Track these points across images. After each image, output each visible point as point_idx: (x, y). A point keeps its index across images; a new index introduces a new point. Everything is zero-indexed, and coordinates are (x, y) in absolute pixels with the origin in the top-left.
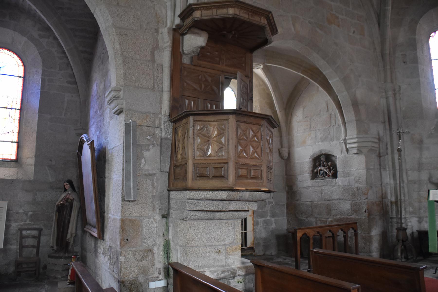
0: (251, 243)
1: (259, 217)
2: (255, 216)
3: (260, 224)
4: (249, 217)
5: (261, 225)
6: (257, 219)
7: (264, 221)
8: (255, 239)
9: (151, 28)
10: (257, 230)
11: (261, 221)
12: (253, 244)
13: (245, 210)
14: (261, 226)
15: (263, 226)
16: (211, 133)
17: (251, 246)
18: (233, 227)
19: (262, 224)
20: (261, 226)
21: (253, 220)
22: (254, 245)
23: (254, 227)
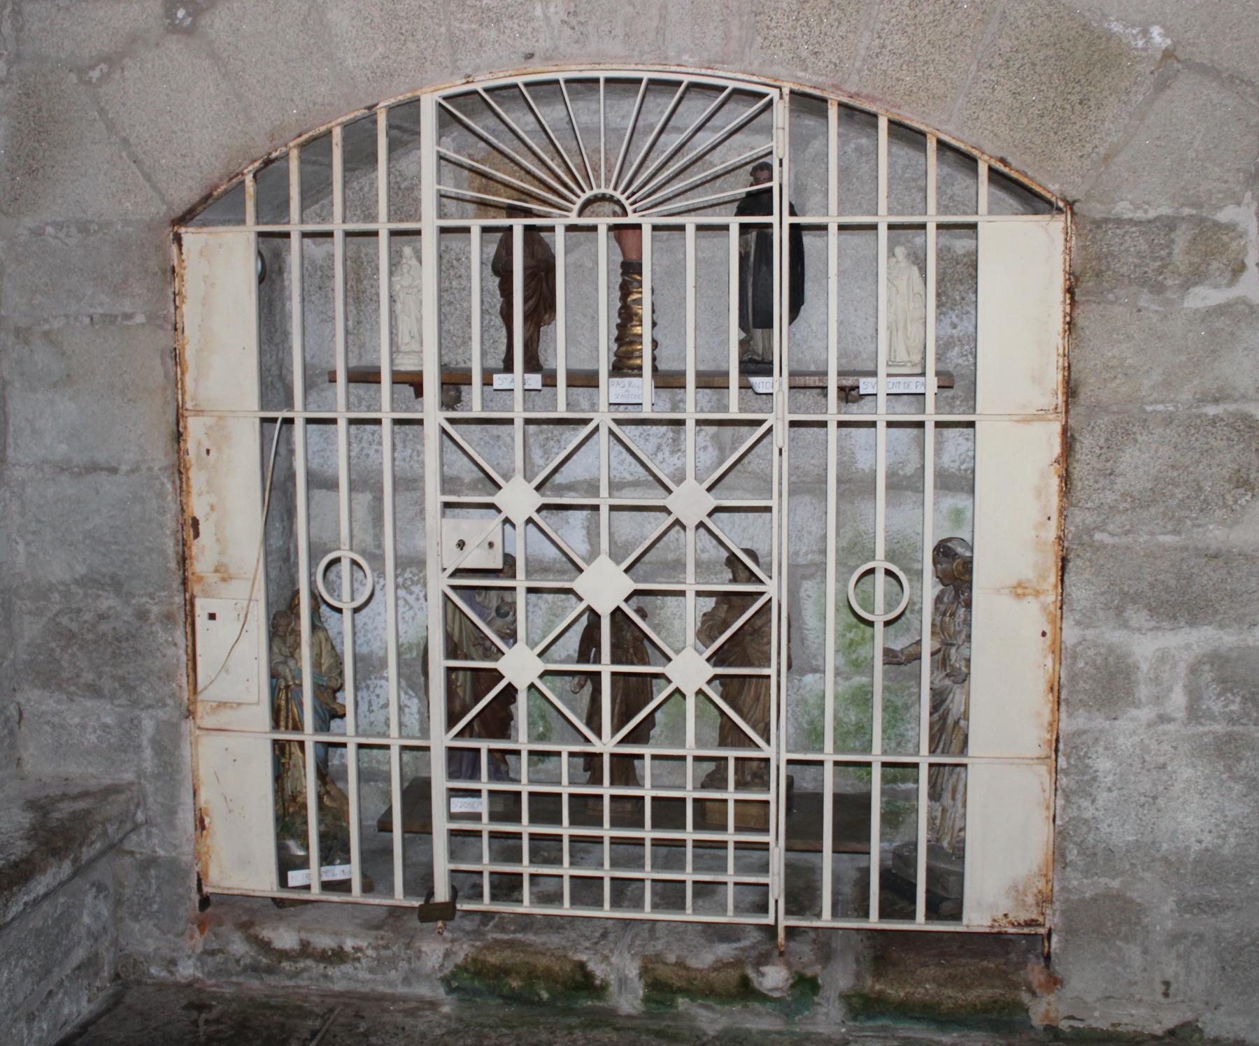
0: (1017, 892)
1: (1137, 617)
2: (1080, 592)
3: (1143, 691)
4: (1007, 601)
5: (1158, 700)
6: (1114, 636)
7: (1217, 659)
8: (1073, 854)
9: (168, 675)
10: (1103, 764)
11: (1163, 657)
12: (1045, 900)
13: (415, 753)
14: (1163, 719)
15: (1194, 713)
16: (188, 848)
17: (1023, 916)
18: (1063, 647)
19: (1178, 700)
20: (1163, 719)
21: (1057, 649)
22: (1053, 919)
23: (1066, 725)
